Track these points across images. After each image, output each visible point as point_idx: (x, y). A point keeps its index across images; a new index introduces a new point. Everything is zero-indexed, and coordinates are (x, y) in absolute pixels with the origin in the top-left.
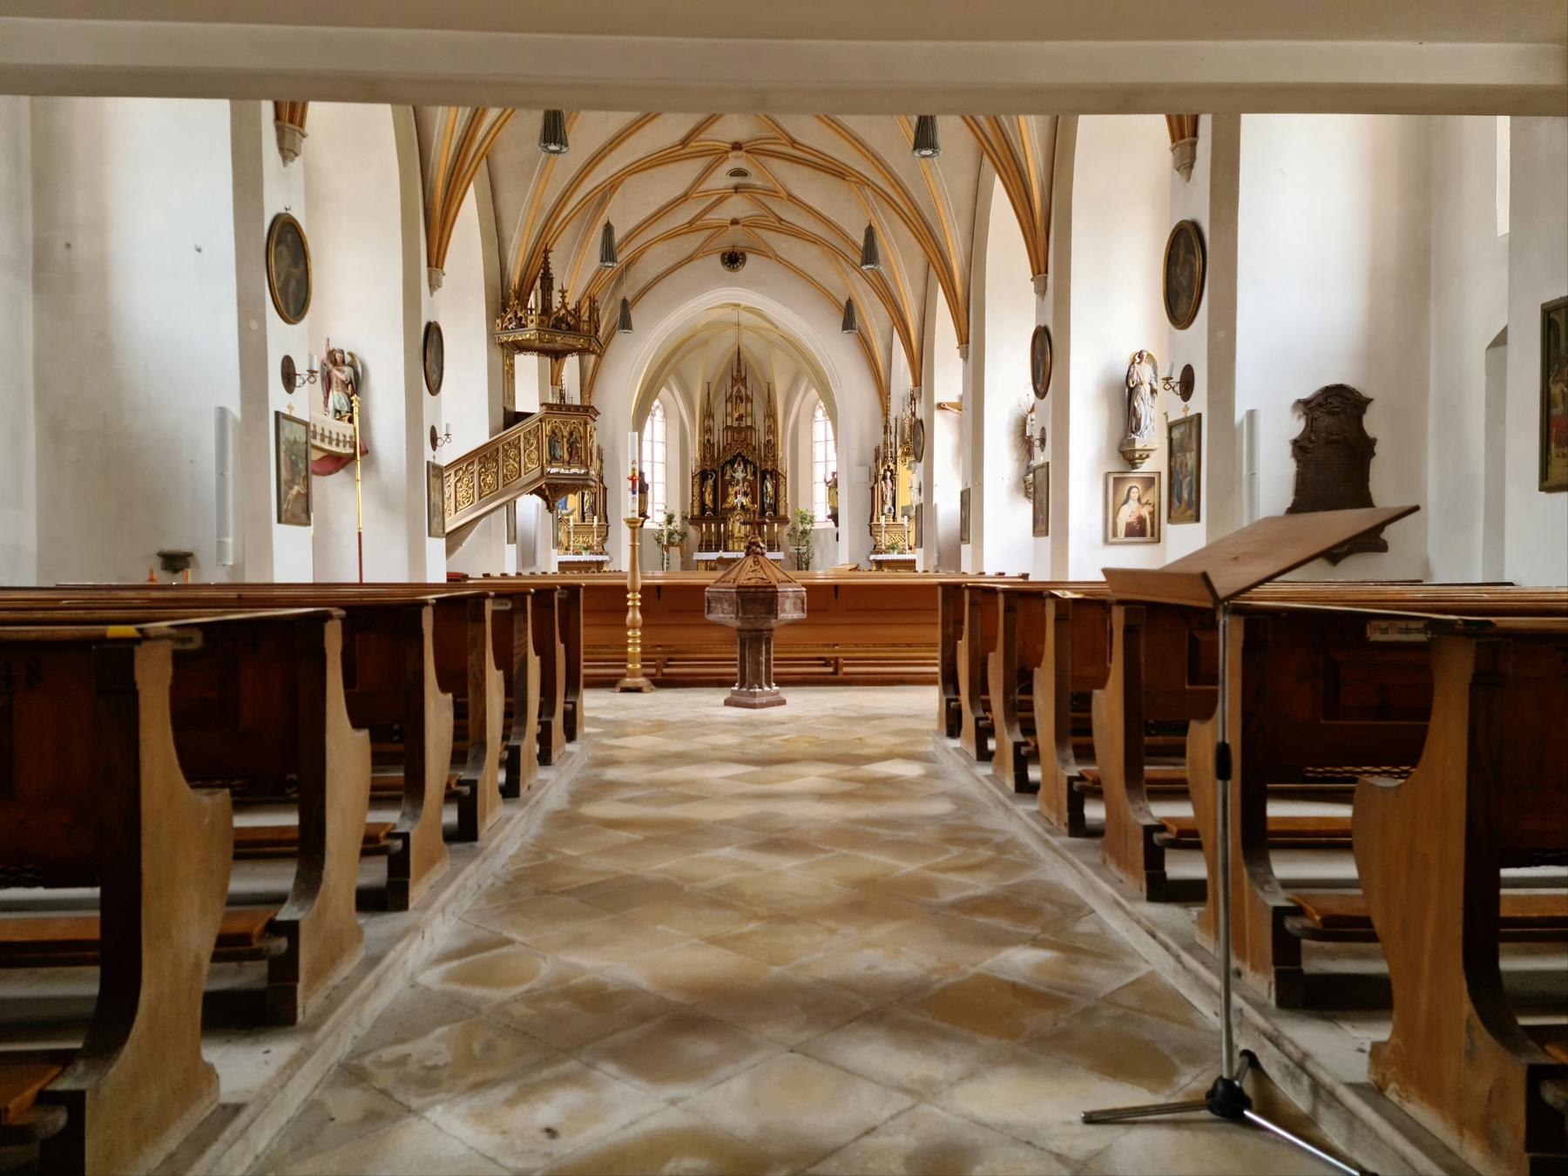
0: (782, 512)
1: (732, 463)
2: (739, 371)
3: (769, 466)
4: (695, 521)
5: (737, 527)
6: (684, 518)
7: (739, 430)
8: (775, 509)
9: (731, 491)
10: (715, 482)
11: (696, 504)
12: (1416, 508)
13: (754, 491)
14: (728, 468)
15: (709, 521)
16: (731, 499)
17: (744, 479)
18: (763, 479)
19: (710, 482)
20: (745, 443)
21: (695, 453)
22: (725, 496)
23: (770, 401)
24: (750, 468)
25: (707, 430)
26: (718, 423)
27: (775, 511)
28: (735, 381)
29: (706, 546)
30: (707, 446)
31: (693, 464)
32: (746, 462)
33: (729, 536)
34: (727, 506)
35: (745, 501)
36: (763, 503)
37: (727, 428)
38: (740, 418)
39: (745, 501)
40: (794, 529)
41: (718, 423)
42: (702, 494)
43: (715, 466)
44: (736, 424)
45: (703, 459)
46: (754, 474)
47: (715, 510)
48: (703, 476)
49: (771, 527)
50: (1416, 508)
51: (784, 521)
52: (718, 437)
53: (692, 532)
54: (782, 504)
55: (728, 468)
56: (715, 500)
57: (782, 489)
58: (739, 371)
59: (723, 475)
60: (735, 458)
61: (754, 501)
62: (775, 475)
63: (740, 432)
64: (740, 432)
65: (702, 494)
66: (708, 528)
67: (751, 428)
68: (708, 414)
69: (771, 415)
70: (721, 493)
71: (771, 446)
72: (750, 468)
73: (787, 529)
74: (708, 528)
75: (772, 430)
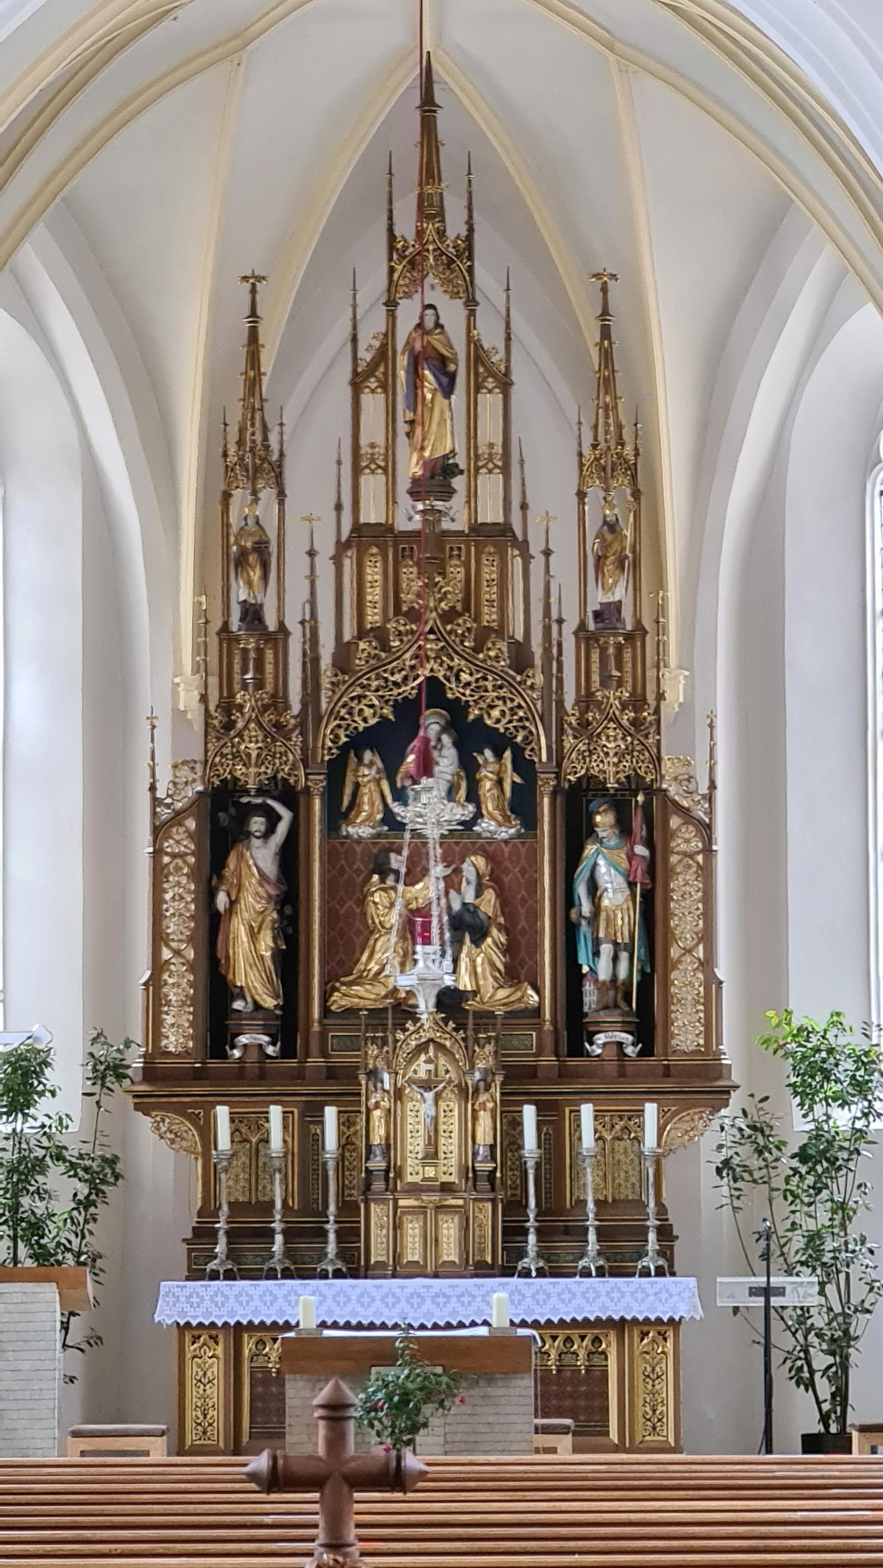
0: (684, 1033)
1: (390, 738)
2: (430, 209)
3: (610, 770)
4: (167, 1087)
5: (429, 1121)
6: (106, 1072)
7: (430, 548)
8: (643, 1007)
9: (387, 906)
10: (290, 857)
11: (179, 986)
12: (84, 1094)
13: (522, 912)
14: (368, 771)
15: (252, 1083)
16: (385, 950)
17: (461, 840)
18: (576, 835)
19: (261, 856)
20: (469, 624)
21: (171, 680)
22: (343, 959)
23: (609, 370)
24: (495, 772)
25: (249, 553)
26: (309, 511)
27: (646, 1027)
28: (407, 263)
29: (231, 1240)
30: (242, 643)
31: (166, 756)
32: (471, 737)
33: (372, 1177)
34: (362, 995)
35: (476, 969)
36: (573, 978)
37: (363, 538)
38: (438, 478)
39: (476, 969)
40: (758, 1132)
41: (309, 511)
42: (212, 926)
43: (288, 764)
44: (409, 517)
45: (222, 720)
46: (522, 806)
47: (286, 1025)
48: (222, 817)
49: (621, 1125)
50: (84, 1094)
51: (700, 1084)
52: (307, 594)
53: (160, 1163)
54: (684, 982)
55: (368, 771)
56: (288, 965)
57: (683, 889)
58: (430, 209)
59: (337, 815)
60: (408, 713)
61: (517, 970)
62: (644, 810)
63: (433, 552)
64: (433, 552)
65: (212, 926)
66: (249, 1127)
67: (499, 537)
68: (251, 460)
69: (618, 462)
70: (319, 925)
71: (619, 641)
72: (495, 772)
73: (715, 1135)
74: (249, 1127)
75: (625, 549)
